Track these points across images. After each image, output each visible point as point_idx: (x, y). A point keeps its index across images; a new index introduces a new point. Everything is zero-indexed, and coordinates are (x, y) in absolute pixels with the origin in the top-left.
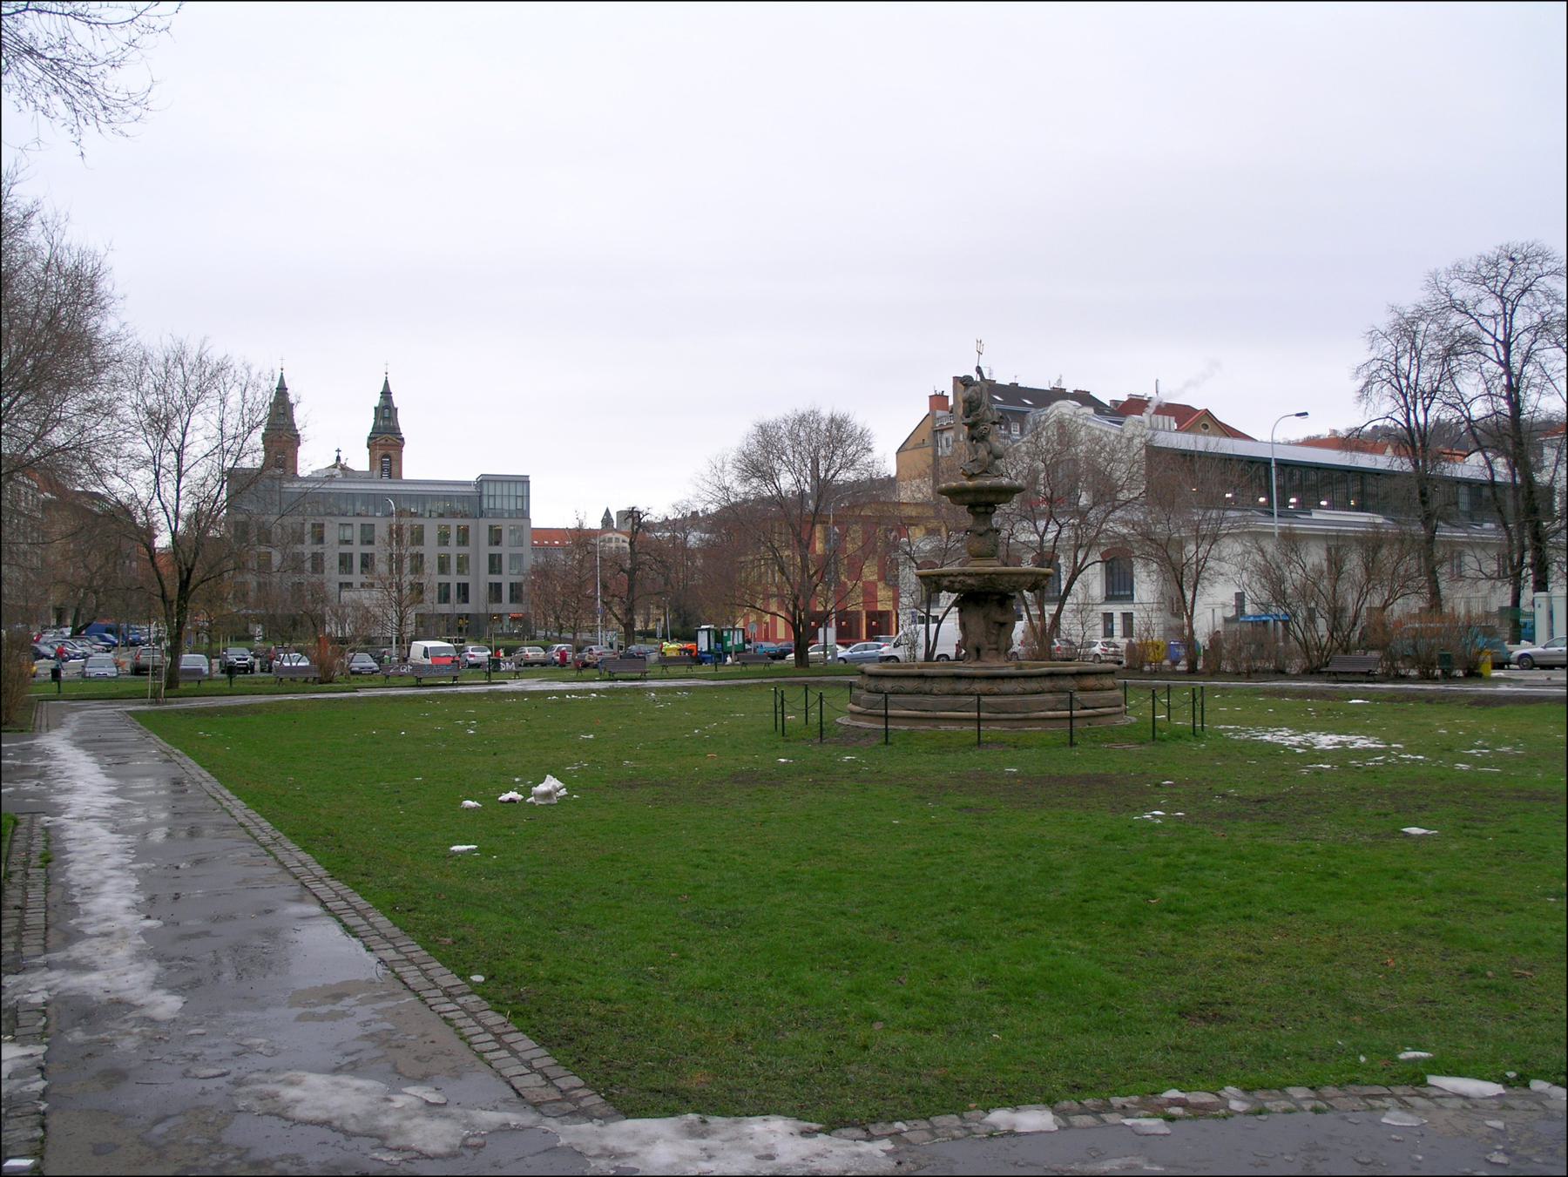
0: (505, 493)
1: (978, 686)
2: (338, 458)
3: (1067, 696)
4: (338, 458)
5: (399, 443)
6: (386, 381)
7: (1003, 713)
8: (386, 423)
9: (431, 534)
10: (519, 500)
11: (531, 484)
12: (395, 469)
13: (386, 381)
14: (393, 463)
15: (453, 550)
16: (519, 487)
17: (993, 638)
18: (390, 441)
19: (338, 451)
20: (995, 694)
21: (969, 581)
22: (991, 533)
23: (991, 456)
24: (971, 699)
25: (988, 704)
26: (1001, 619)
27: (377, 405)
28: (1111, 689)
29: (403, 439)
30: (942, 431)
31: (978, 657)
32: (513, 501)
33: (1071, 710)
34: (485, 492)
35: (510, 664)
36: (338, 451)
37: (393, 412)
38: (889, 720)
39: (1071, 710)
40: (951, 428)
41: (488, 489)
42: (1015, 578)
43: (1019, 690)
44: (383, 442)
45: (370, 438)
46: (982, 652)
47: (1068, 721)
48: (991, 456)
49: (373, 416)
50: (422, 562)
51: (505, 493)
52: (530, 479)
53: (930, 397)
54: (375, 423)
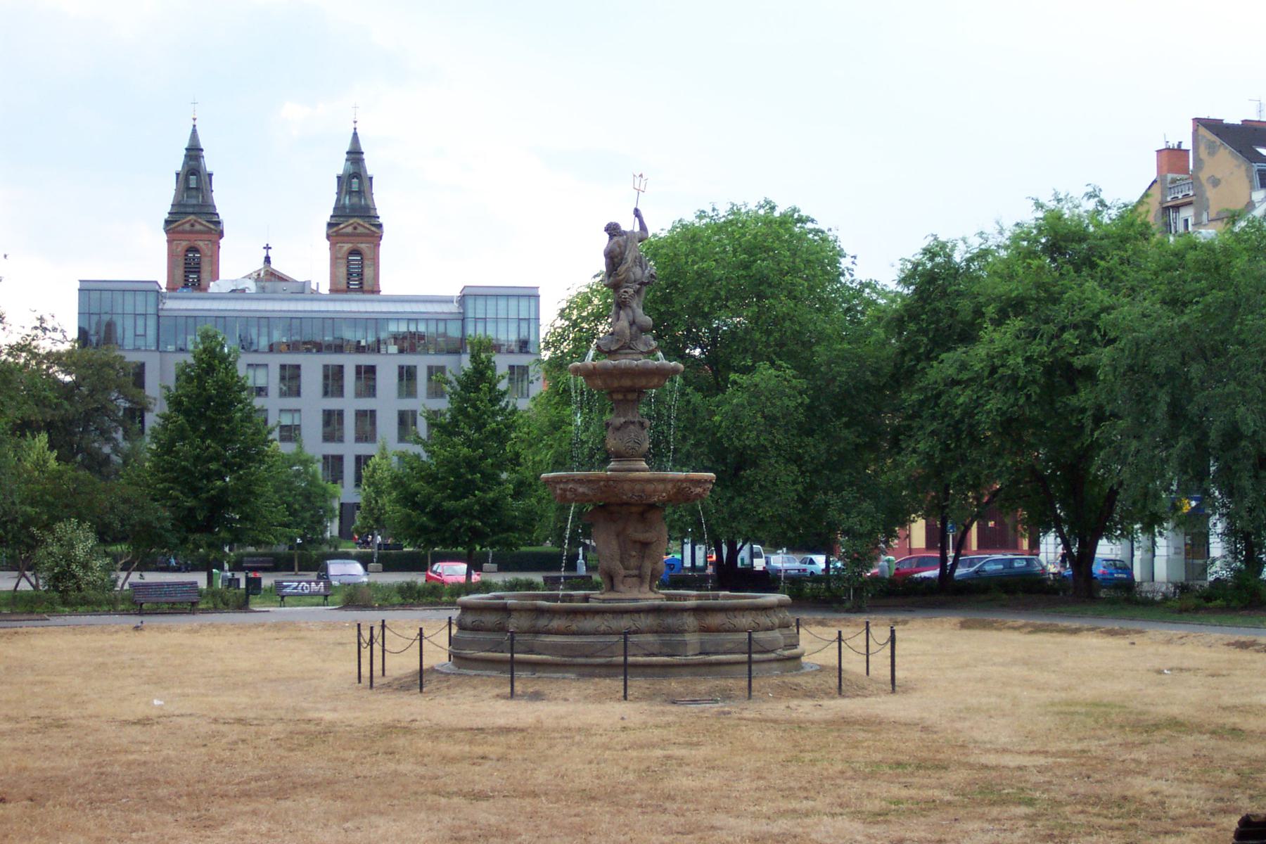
0: (513, 315)
1: (625, 623)
2: (267, 260)
3: (746, 635)
4: (267, 260)
5: (374, 232)
6: (355, 134)
7: (581, 656)
8: (355, 200)
9: (387, 379)
10: (524, 325)
11: (541, 299)
12: (368, 272)
13: (355, 134)
14: (366, 262)
15: (349, 403)
16: (524, 303)
17: (633, 562)
18: (360, 230)
19: (268, 248)
20: (574, 633)
21: (581, 490)
22: (632, 427)
23: (634, 328)
24: (615, 639)
25: (637, 645)
26: (641, 536)
27: (341, 172)
28: (768, 629)
29: (380, 226)
30: (1177, 208)
31: (612, 588)
32: (513, 327)
33: (750, 653)
34: (470, 314)
35: (317, 584)
36: (268, 248)
37: (366, 183)
38: (629, 670)
39: (750, 653)
40: (1190, 203)
41: (476, 309)
42: (638, 487)
43: (603, 628)
44: (350, 230)
45: (330, 225)
46: (615, 579)
47: (746, 667)
48: (634, 328)
49: (335, 189)
50: (373, 423)
51: (502, 314)
52: (540, 292)
53: (1159, 152)
54: (338, 200)
